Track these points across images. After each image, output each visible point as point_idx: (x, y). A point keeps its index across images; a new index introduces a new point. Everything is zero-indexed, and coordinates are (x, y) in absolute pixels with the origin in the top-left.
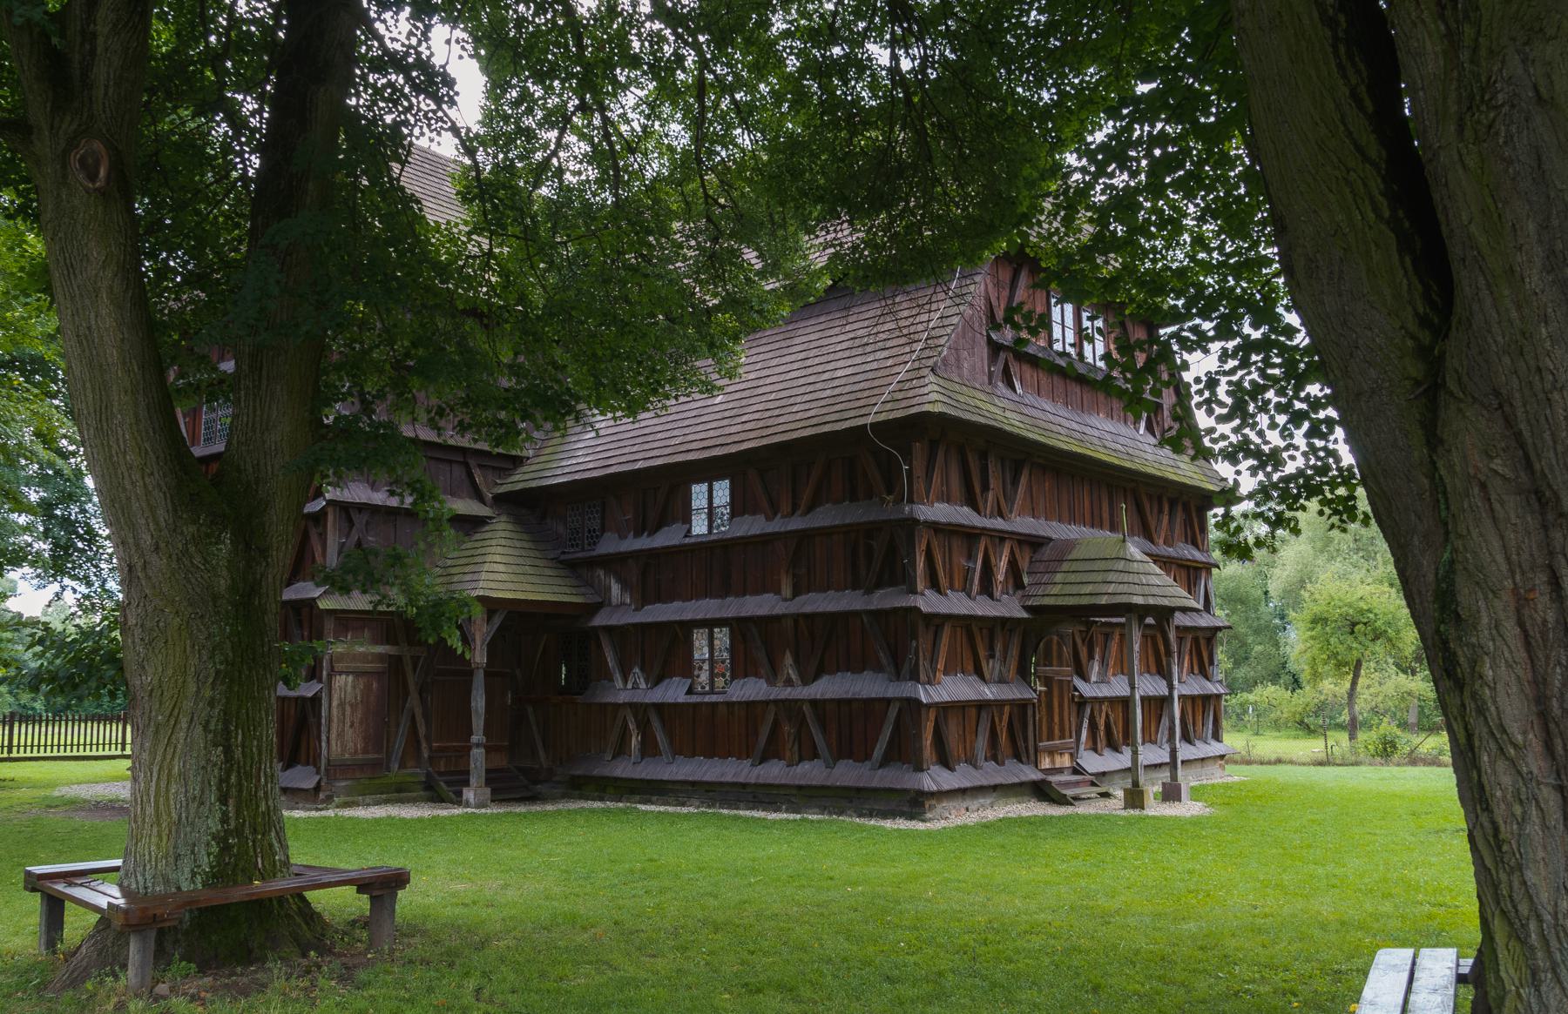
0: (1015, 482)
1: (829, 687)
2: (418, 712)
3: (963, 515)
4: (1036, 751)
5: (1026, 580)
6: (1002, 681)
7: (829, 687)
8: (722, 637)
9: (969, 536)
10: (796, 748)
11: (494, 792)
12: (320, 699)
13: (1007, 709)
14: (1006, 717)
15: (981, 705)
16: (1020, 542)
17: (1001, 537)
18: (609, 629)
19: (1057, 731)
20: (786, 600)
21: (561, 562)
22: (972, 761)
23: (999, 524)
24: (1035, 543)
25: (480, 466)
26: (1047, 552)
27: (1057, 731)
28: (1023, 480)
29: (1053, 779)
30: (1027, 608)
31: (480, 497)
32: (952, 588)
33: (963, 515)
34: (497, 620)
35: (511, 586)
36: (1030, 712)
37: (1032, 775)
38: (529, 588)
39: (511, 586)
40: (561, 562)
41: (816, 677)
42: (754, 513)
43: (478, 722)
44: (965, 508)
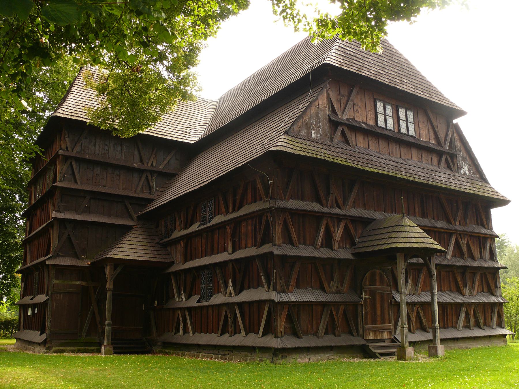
0: (351, 191)
1: (248, 296)
2: (96, 312)
3: (315, 207)
4: (363, 329)
5: (357, 240)
6: (338, 292)
7: (248, 296)
8: (429, 300)
9: (318, 217)
10: (233, 327)
11: (114, 348)
12: (47, 304)
13: (342, 307)
14: (341, 312)
15: (324, 305)
16: (460, 235)
17: (339, 218)
18: (173, 273)
19: (379, 319)
20: (230, 254)
21: (160, 244)
22: (316, 334)
23: (337, 211)
24: (366, 222)
25: (131, 204)
26: (371, 226)
27: (379, 319)
28: (355, 190)
29: (371, 345)
30: (353, 254)
31: (132, 219)
32: (300, 244)
33: (315, 207)
34: (119, 270)
35: (143, 255)
36: (359, 310)
37: (357, 341)
38: (139, 255)
39: (143, 255)
40: (160, 244)
41: (240, 292)
42: (221, 214)
43: (108, 315)
44: (315, 203)
